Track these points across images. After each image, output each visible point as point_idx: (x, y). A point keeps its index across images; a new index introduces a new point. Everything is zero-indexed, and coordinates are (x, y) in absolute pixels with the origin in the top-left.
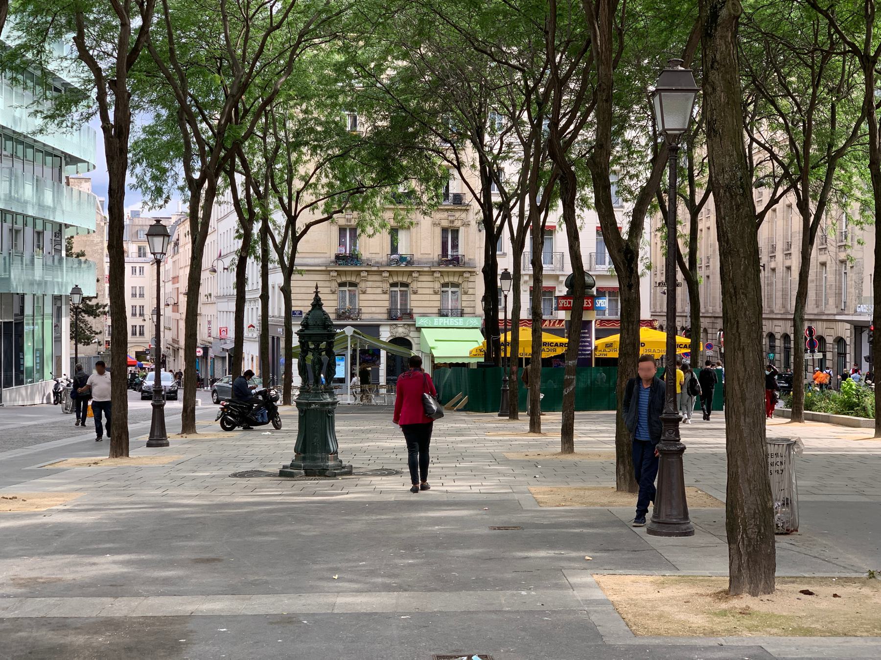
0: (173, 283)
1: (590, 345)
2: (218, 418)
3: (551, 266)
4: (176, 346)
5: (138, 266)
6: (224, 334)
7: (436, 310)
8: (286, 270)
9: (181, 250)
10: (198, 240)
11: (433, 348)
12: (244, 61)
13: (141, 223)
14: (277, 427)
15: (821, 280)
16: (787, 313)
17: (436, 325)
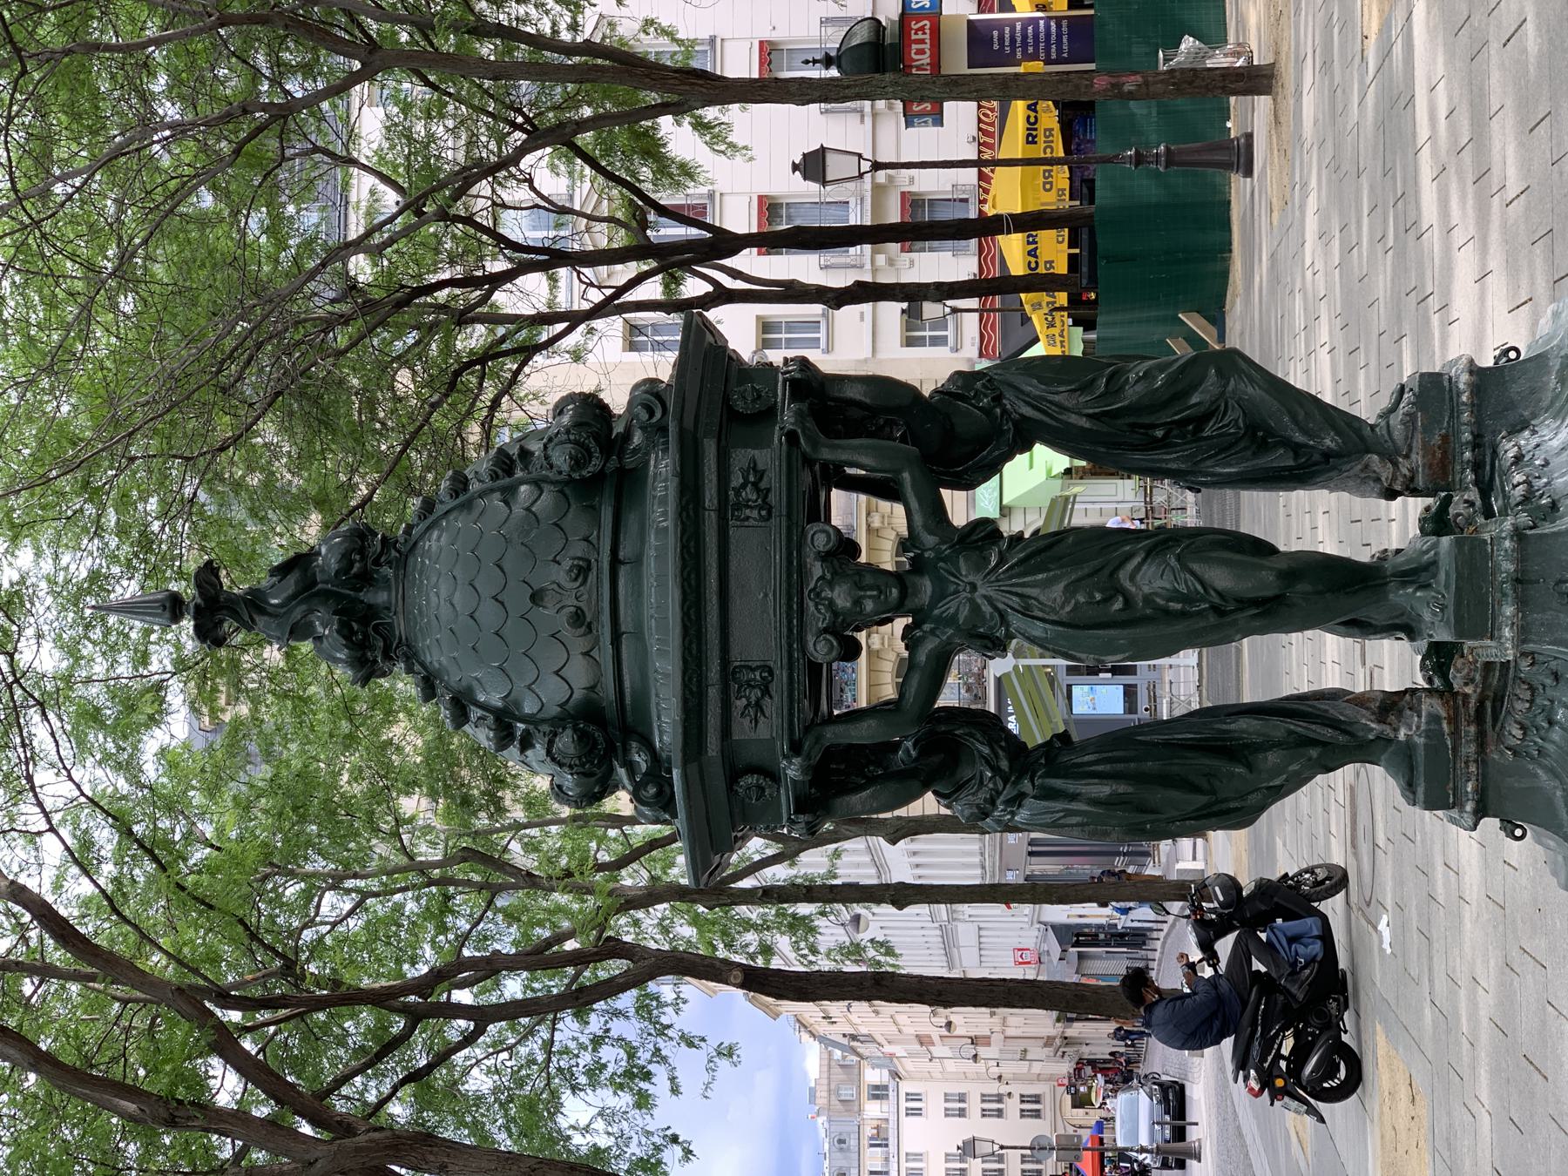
0: (933, 1044)
3: (852, 205)
4: (1058, 1041)
5: (904, 1105)
6: (1028, 956)
8: (843, 829)
9: (864, 1030)
11: (1049, 471)
12: (196, 971)
13: (825, 1094)
14: (1337, 881)
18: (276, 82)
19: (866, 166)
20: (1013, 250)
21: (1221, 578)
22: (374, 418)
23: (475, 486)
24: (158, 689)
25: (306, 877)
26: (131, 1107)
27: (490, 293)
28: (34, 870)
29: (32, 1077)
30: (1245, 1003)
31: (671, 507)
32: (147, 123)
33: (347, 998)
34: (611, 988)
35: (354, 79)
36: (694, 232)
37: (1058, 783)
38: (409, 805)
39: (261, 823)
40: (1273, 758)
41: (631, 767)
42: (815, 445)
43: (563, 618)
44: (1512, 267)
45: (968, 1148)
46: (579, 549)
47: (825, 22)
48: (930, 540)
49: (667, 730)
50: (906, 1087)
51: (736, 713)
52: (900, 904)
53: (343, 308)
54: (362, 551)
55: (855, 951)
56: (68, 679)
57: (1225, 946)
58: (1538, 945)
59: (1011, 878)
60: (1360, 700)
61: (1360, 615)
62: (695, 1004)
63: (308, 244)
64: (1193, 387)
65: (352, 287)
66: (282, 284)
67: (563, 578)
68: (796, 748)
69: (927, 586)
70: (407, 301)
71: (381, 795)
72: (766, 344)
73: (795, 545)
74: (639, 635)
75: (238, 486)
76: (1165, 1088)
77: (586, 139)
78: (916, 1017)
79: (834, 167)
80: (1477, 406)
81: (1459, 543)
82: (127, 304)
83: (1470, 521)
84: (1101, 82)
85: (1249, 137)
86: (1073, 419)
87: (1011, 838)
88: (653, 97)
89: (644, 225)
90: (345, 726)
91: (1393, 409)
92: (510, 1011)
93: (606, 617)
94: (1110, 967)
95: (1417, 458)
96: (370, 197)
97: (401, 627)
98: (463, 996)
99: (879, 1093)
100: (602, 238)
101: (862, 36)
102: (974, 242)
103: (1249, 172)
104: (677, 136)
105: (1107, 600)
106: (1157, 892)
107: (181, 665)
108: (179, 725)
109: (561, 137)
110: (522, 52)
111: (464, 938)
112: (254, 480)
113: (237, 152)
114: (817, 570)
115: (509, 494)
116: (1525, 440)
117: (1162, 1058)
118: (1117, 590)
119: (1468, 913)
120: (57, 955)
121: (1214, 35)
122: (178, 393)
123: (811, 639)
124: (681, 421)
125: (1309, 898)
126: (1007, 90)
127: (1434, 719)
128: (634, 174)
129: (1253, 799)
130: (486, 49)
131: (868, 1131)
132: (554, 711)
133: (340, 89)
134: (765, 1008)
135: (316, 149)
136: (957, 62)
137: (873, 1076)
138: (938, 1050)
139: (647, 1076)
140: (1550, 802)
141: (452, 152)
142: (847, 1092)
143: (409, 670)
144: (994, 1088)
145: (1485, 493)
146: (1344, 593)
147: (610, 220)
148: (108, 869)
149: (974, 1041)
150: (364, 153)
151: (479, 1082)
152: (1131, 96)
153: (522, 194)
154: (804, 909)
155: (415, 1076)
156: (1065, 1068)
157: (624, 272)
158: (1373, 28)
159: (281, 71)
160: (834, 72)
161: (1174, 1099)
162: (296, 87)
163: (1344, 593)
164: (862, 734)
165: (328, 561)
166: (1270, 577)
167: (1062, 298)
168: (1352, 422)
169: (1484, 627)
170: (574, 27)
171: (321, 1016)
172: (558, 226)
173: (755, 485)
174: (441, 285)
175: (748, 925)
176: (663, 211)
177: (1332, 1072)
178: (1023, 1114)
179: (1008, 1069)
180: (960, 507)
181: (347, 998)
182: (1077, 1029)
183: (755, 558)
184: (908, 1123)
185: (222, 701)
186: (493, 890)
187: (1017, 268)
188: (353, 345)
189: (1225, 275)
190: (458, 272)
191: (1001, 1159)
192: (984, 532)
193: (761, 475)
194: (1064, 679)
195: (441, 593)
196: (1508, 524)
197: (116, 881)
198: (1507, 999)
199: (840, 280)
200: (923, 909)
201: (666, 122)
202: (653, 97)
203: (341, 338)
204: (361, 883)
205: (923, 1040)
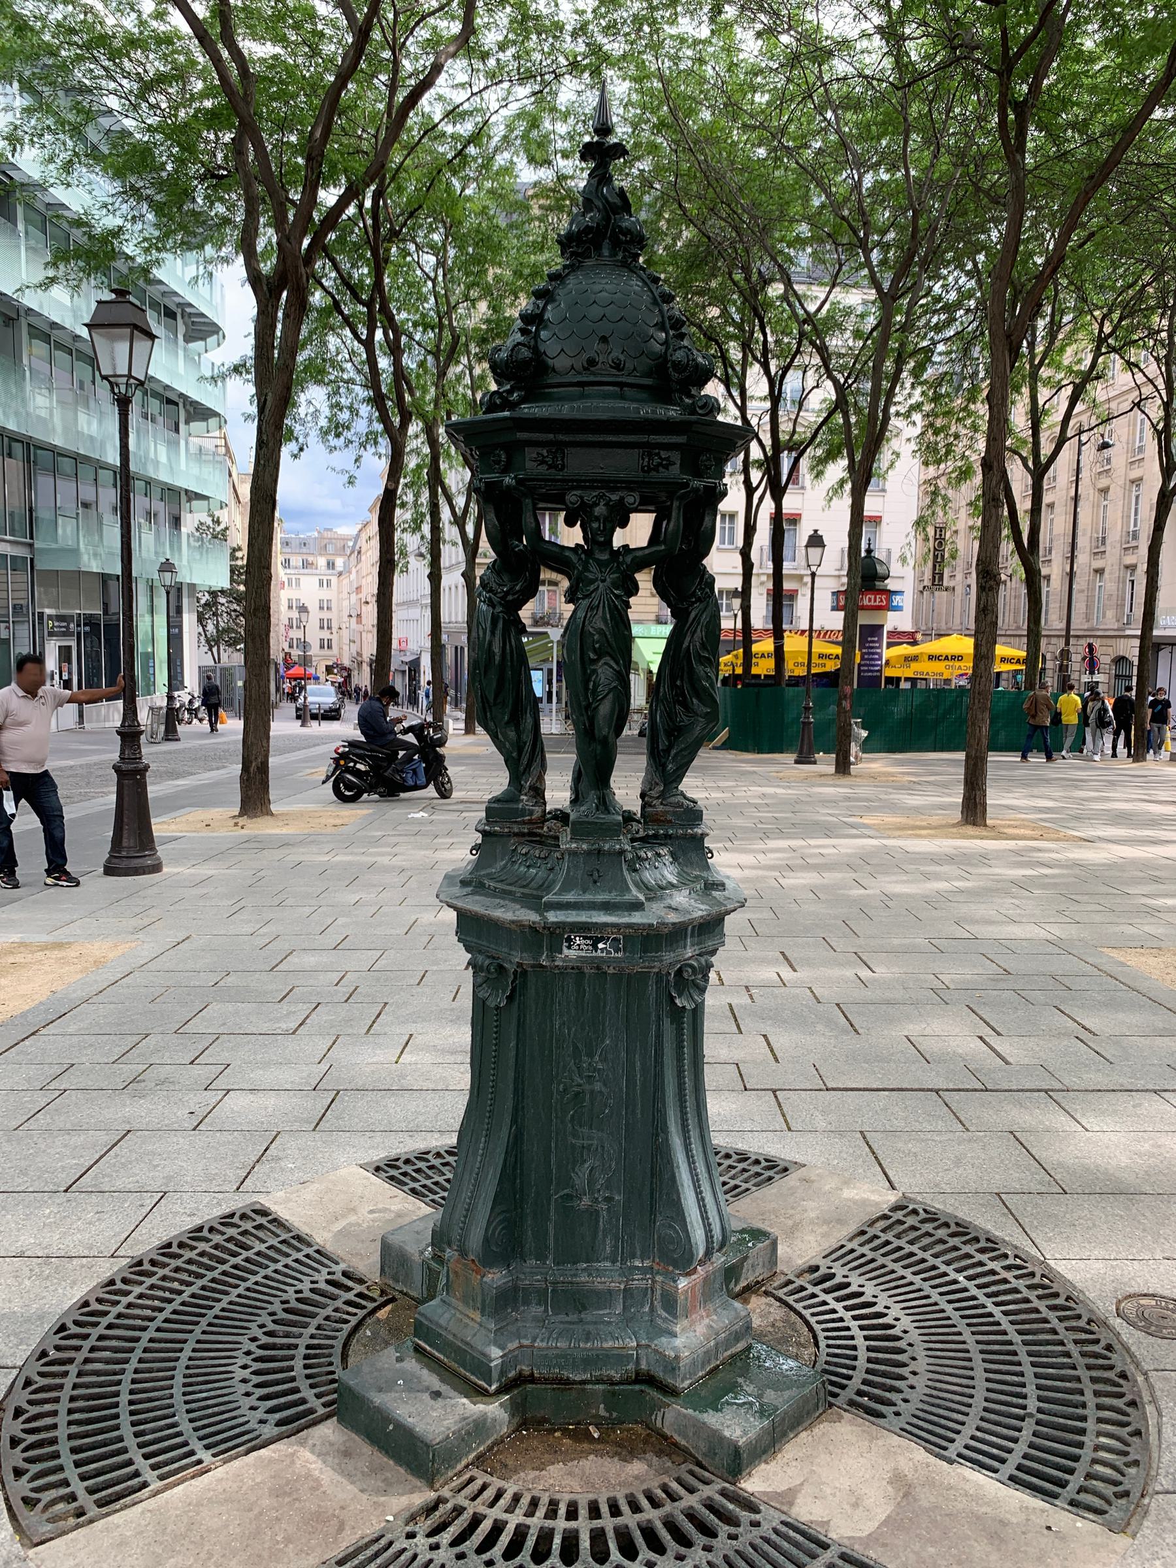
1: (880, 659)
2: (328, 778)
7: (653, 617)
10: (269, 404)
14: (444, 793)
15: (1093, 589)
16: (1018, 628)
17: (653, 634)
18: (878, 244)
19: (814, 569)
20: (765, 646)
21: (605, 709)
22: (694, 294)
23: (665, 307)
24: (547, 162)
25: (444, 245)
26: (318, 134)
27: (759, 362)
28: (450, 82)
29: (332, 79)
30: (382, 747)
31: (650, 416)
32: (861, 165)
33: (379, 265)
34: (384, 418)
35: (879, 290)
36: (784, 478)
37: (500, 625)
38: (483, 306)
39: (472, 221)
40: (512, 734)
41: (510, 392)
42: (681, 498)
43: (593, 354)
44: (746, 880)
45: (303, 609)
46: (629, 365)
47: (889, 552)
48: (629, 559)
49: (529, 410)
50: (334, 579)
51: (540, 450)
52: (430, 576)
53: (755, 277)
54: (631, 242)
55: (404, 554)
56: (554, 109)
57: (411, 738)
58: (413, 883)
59: (444, 637)
60: (541, 778)
61: (584, 778)
62: (377, 464)
63: (790, 260)
64: (700, 700)
65: (766, 282)
66: (769, 242)
67: (614, 354)
68: (520, 482)
69: (605, 557)
70: (757, 315)
71: (487, 292)
72: (723, 516)
73: (629, 486)
74: (582, 396)
75: (659, 215)
76: (338, 710)
77: (839, 419)
78: (371, 585)
79: (814, 552)
80: (685, 837)
81: (618, 824)
82: (762, 152)
83: (629, 831)
84: (848, 689)
85: (815, 763)
86: (688, 639)
87: (464, 638)
88: (858, 457)
89: (790, 450)
90: (526, 271)
91: (685, 797)
92: (372, 361)
93: (592, 378)
94: (400, 684)
95: (661, 808)
96: (814, 298)
97: (589, 263)
98: (379, 335)
99: (331, 565)
100: (785, 427)
101: (880, 569)
102: (771, 626)
103: (797, 762)
104: (837, 470)
105: (595, 651)
106: (437, 708)
107: (561, 178)
108: (527, 175)
109: (841, 404)
110: (885, 385)
111: (411, 337)
112: (663, 224)
113: (843, 218)
114: (615, 497)
115: (661, 327)
116: (668, 859)
117: (352, 711)
118: (600, 654)
119: (429, 853)
120: (400, 97)
121: (866, 747)
122: (710, 177)
123: (578, 493)
124: (696, 422)
125: (435, 780)
126: (847, 643)
127: (531, 813)
128: (819, 445)
129: (491, 724)
130: (889, 365)
131: (310, 559)
132: (542, 348)
133: (875, 283)
134: (374, 506)
135: (841, 265)
136: (863, 619)
137: (339, 562)
138: (354, 597)
139: (338, 436)
140: (490, 866)
141: (835, 342)
142: (330, 548)
143: (565, 267)
144: (335, 625)
145: (641, 839)
146: (594, 774)
147: (794, 431)
148: (449, 129)
149: (359, 616)
150: (838, 294)
151: (333, 341)
152: (839, 705)
153: (811, 381)
154: (426, 528)
155: (336, 305)
156: (346, 663)
157: (767, 440)
158: (865, 821)
159: (885, 248)
160: (863, 554)
161: (332, 715)
162: (875, 256)
163: (594, 774)
164: (528, 519)
165: (626, 222)
166: (605, 732)
167: (739, 671)
168: (680, 778)
169: (576, 835)
170: (898, 414)
171: (369, 254)
172: (793, 402)
173: (660, 464)
174: (765, 335)
175: (417, 495)
176: (797, 460)
177: (348, 788)
178: (322, 640)
179: (345, 633)
180: (645, 579)
181: (379, 265)
182: (366, 669)
183: (623, 463)
184: (315, 580)
185: (541, 202)
186: (436, 354)
187: (756, 648)
188: (735, 284)
189: (747, 750)
190: (771, 346)
191: (298, 627)
192: (634, 589)
193: (666, 467)
194: (546, 667)
195: (605, 286)
196: (627, 847)
197: (444, 134)
198: (386, 869)
199: (754, 556)
200: (428, 591)
201: (844, 462)
202: (858, 457)
203: (738, 276)
204: (440, 278)
205: (358, 589)
